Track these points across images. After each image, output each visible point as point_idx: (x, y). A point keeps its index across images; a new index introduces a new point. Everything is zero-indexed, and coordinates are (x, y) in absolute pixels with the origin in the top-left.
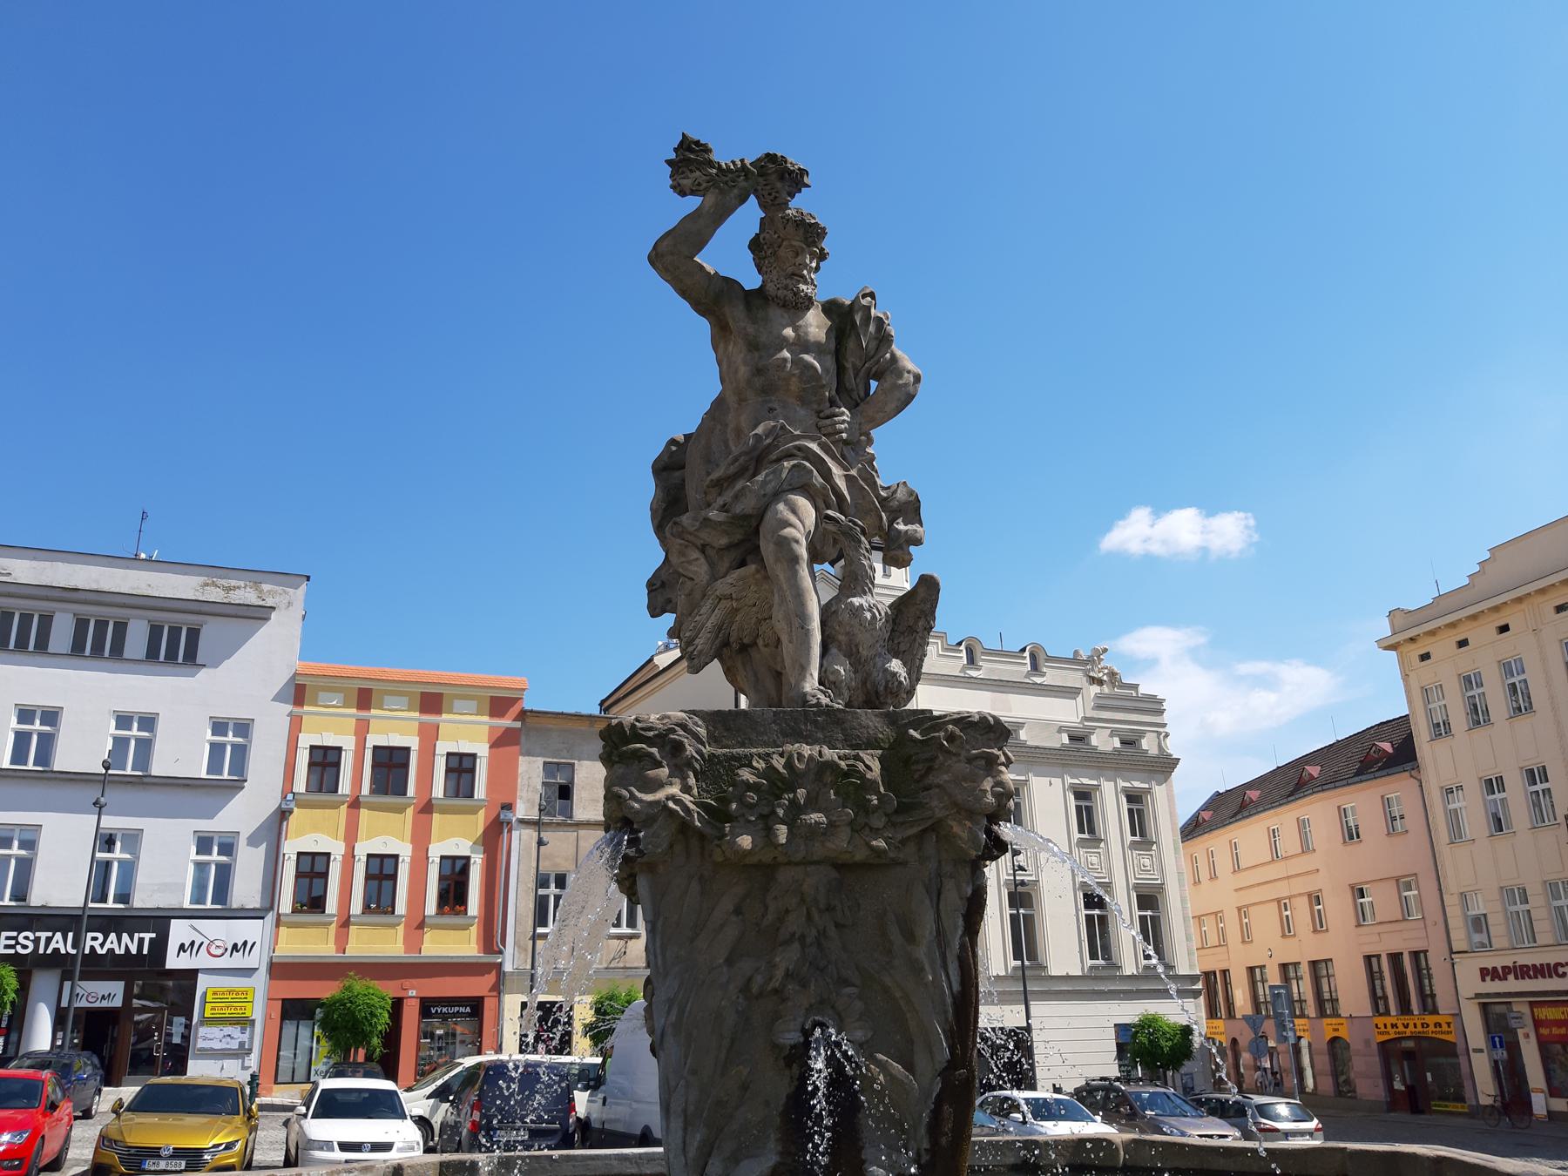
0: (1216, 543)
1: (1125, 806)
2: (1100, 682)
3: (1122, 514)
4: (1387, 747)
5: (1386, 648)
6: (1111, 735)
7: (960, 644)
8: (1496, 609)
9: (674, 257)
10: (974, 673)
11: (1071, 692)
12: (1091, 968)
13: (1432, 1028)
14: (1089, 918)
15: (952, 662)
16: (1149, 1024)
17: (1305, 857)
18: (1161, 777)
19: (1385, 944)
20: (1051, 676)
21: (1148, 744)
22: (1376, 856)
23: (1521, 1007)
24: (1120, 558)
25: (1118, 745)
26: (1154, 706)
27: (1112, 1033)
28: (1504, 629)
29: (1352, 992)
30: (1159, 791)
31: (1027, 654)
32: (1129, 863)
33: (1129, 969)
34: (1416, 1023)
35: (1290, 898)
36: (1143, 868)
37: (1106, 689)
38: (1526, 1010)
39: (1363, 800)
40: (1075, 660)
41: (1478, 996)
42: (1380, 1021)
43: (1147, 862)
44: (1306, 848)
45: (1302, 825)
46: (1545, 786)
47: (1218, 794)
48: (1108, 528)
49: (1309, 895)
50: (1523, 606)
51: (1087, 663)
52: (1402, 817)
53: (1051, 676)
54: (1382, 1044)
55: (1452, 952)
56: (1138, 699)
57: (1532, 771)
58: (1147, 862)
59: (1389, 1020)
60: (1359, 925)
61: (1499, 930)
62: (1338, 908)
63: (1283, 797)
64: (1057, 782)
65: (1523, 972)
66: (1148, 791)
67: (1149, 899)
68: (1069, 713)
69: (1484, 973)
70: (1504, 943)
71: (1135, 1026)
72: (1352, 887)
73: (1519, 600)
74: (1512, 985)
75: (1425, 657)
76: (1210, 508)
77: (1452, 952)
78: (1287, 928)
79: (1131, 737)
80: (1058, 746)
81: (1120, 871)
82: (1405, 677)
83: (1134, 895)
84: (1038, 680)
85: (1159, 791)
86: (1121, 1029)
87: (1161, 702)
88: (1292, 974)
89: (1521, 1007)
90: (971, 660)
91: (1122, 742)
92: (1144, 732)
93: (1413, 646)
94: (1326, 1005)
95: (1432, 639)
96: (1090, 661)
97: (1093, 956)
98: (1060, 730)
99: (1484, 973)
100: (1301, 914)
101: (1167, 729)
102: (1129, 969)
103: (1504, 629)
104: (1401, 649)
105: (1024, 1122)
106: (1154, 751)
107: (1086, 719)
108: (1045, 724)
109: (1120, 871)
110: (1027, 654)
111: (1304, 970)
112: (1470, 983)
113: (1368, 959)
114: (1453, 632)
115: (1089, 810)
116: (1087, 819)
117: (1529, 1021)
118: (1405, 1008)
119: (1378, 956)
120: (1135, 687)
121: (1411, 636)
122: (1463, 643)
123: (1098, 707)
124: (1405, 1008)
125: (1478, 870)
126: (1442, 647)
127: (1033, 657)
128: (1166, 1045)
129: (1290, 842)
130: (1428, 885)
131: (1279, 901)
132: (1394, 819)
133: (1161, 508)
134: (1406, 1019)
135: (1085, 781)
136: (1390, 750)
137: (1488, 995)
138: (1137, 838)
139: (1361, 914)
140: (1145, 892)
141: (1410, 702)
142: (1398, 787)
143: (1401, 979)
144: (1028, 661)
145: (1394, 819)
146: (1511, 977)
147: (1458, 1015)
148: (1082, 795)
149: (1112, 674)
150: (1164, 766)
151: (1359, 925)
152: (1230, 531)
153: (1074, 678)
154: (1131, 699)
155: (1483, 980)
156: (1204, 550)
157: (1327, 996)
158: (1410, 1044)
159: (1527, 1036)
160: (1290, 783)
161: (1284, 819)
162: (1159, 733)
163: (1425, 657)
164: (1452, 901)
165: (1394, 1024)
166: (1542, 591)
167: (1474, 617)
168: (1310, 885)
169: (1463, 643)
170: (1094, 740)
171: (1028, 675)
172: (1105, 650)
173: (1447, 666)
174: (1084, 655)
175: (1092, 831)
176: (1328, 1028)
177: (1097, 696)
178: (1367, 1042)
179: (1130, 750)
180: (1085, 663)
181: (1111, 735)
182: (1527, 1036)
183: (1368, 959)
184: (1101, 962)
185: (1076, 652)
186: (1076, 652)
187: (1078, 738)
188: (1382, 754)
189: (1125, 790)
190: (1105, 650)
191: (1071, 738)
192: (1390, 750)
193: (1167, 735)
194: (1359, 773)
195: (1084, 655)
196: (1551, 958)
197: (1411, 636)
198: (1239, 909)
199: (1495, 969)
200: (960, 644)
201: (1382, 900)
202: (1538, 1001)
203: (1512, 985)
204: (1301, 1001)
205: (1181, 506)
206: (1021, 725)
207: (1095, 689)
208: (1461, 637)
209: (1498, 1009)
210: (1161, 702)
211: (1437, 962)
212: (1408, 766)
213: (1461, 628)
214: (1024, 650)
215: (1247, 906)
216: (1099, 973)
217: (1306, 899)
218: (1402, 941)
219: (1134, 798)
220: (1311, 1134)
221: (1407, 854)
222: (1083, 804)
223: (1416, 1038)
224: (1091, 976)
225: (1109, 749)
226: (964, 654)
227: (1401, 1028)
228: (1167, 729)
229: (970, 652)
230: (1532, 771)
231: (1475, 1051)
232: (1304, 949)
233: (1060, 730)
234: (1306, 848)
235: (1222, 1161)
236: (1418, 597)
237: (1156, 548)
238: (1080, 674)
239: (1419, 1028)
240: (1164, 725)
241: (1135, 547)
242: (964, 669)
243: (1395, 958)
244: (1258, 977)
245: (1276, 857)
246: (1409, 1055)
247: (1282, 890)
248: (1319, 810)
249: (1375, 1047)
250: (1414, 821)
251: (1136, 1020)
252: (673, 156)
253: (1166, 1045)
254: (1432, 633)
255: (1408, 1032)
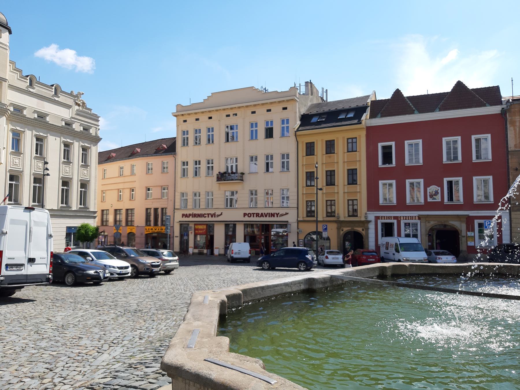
0: (80, 65)
2: (79, 105)
3: (48, 45)
4: (165, 146)
6: (80, 126)
7: (27, 76)
8: (210, 111)
11: (68, 107)
12: (61, 207)
14: (63, 190)
15: (23, 83)
17: (132, 177)
20: (62, 99)
21: (92, 131)
22: (157, 178)
23: (192, 225)
24: (42, 60)
25: (82, 129)
27: (65, 229)
28: (210, 118)
29: (139, 219)
30: (93, 148)
31: (54, 88)
32: (80, 172)
33: (74, 208)
35: (123, 189)
37: (81, 108)
38: (193, 226)
39: (156, 161)
40: (71, 94)
41: (180, 222)
42: (147, 228)
43: (86, 172)
44: (132, 174)
45: (132, 166)
49: (131, 189)
50: (218, 112)
52: (152, 169)
53: (62, 99)
54: (146, 235)
55: (175, 209)
58: (86, 172)
59: (150, 228)
61: (190, 205)
62: (140, 193)
64: (58, 139)
65: (195, 215)
67: (84, 185)
68: (66, 114)
69: (183, 215)
70: (191, 207)
71: (79, 227)
72: (146, 187)
73: (217, 110)
74: (191, 219)
75: (185, 121)
76: (80, 53)
78: (120, 198)
79: (87, 127)
80: (60, 126)
81: (76, 174)
82: (178, 126)
84: (57, 99)
85: (93, 148)
86: (69, 228)
89: (192, 225)
90: (31, 84)
91: (84, 129)
92: (92, 127)
93: (182, 117)
97: (62, 203)
98: (62, 120)
99: (183, 215)
100: (126, 194)
101: (99, 127)
102: (74, 208)
103: (210, 118)
104: (178, 117)
105: (93, 260)
106: (94, 134)
107: (72, 118)
108: (56, 116)
109: (76, 174)
111: (124, 212)
112: (178, 217)
113: (147, 209)
114: (195, 115)
115: (68, 151)
117: (193, 229)
118: (156, 224)
119: (150, 209)
120: (90, 110)
121: (182, 114)
122: (197, 119)
123: (77, 114)
124: (156, 224)
125: (187, 185)
126: (191, 119)
127: (56, 89)
129: (127, 171)
130: (171, 190)
131: (118, 189)
132: (149, 169)
133: (62, 47)
134: (156, 227)
135: (69, 140)
137: (183, 222)
138: (83, 164)
139: (147, 196)
140: (83, 182)
141: (177, 134)
142: (168, 159)
143: (155, 216)
145: (149, 169)
146: (191, 217)
147: (173, 227)
148: (67, 145)
149: (84, 103)
150: (96, 140)
152: (86, 63)
153: (69, 101)
154: (88, 113)
155: (244, 217)
156: (75, 67)
158: (156, 235)
159: (191, 233)
160: (129, 152)
161: (127, 164)
162: (96, 128)
163: (185, 121)
165: (152, 229)
166: (224, 109)
167: (203, 112)
168: (131, 186)
169: (197, 119)
170: (74, 126)
172: (83, 94)
173: (191, 126)
174: (75, 93)
175: (68, 159)
176: (128, 230)
177: (77, 110)
178: (142, 234)
179: (85, 131)
181: (80, 126)
182: (191, 233)
183: (147, 209)
186: (72, 92)
187: (68, 124)
188: (166, 148)
189: (82, 146)
190: (83, 94)
191: (66, 124)
193: (99, 129)
194: (155, 153)
195: (75, 93)
196: (203, 212)
197: (182, 114)
198: (102, 191)
199: (187, 214)
200: (27, 76)
201: (155, 193)
202: (196, 223)
203: (191, 219)
204: (120, 221)
205: (71, 49)
207: (77, 107)
208: (197, 118)
209: (185, 225)
210: (99, 117)
211: (169, 212)
212: (173, 153)
213: (197, 115)
214: (53, 85)
217: (117, 191)
218: (159, 205)
219: (85, 149)
220: (176, 260)
221: (167, 180)
222: (66, 149)
224: (61, 209)
226: (28, 81)
227: (154, 230)
228: (99, 127)
231: (176, 237)
232: (124, 205)
233: (62, 120)
234: (132, 174)
236: (186, 103)
237: (56, 60)
238: (72, 101)
239: (160, 230)
240: (98, 126)
241: (48, 58)
242: (27, 87)
243: (156, 210)
244: (164, 212)
245: (121, 175)
246: (154, 238)
247: (121, 186)
248: (139, 164)
249: (144, 235)
250: (171, 169)
254: (189, 114)
255: (156, 231)
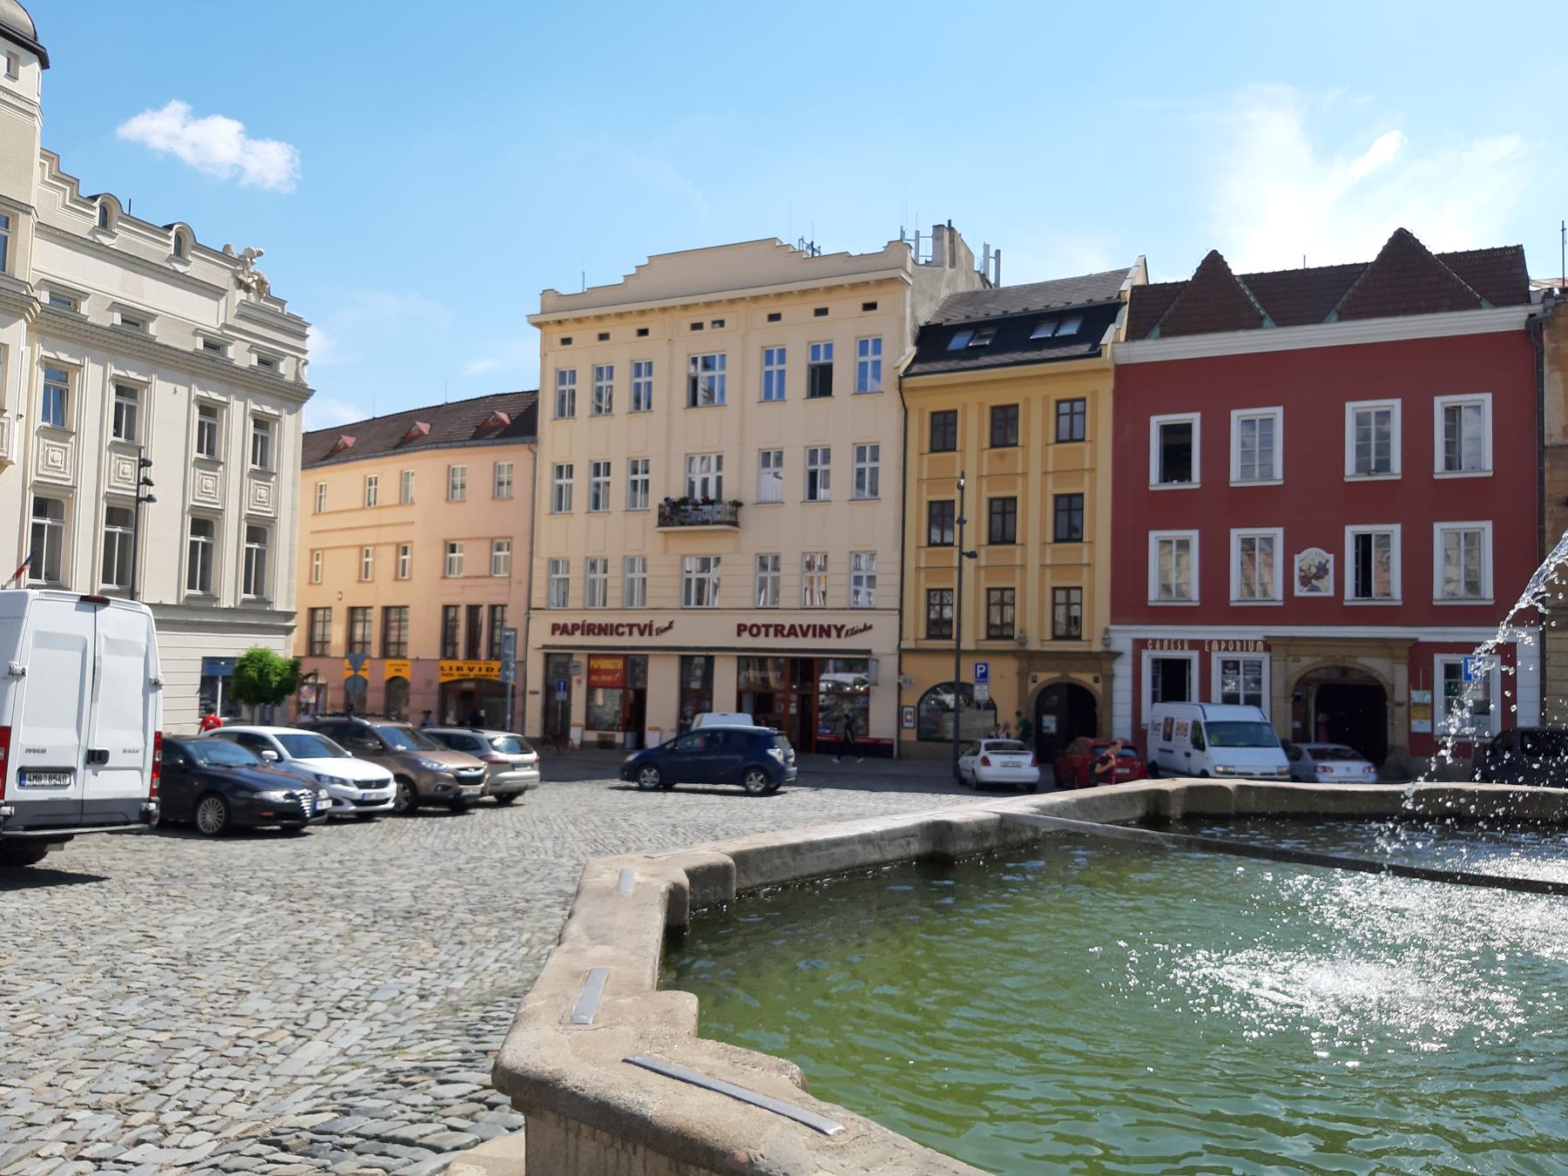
0: (253, 166)
1: (251, 430)
2: (247, 288)
3: (158, 105)
4: (504, 417)
5: (535, 324)
6: (250, 351)
7: (94, 198)
8: (642, 313)
10: (106, 241)
11: (216, 292)
12: (189, 598)
13: (496, 672)
14: (194, 545)
15: (79, 219)
16: (257, 660)
17: (402, 509)
18: (293, 406)
19: (463, 596)
20: (196, 268)
21: (286, 368)
22: (477, 516)
23: (580, 658)
24: (139, 148)
26: (297, 328)
27: (198, 666)
28: (643, 332)
29: (422, 638)
30: (288, 420)
31: (172, 234)
33: (227, 601)
34: (484, 667)
35: (375, 545)
36: (259, 499)
37: (253, 298)
38: (584, 660)
39: (476, 464)
40: (224, 255)
41: (545, 647)
42: (447, 664)
44: (405, 500)
45: (405, 477)
46: (607, 479)
48: (135, 111)
49: (398, 545)
50: (666, 316)
51: (237, 262)
52: (463, 486)
53: (196, 268)
54: (443, 686)
55: (530, 608)
56: (281, 317)
57: (636, 462)
58: (263, 493)
59: (455, 664)
60: (360, 581)
61: (576, 596)
62: (425, 560)
63: (388, 448)
64: (183, 390)
65: (589, 629)
66: (277, 418)
67: (258, 531)
68: (208, 315)
69: (555, 628)
71: (242, 660)
72: (445, 542)
73: (664, 310)
74: (578, 639)
76: (255, 130)
77: (530, 608)
78: (364, 573)
79: (269, 356)
80: (191, 350)
82: (544, 356)
83: (244, 526)
85: (288, 420)
86: (210, 662)
87: (305, 325)
88: (360, 617)
91: (260, 361)
92: (285, 355)
93: (557, 328)
94: (391, 648)
95: (578, 326)
96: (241, 261)
97: (191, 586)
98: (196, 333)
99: (555, 628)
100: (385, 562)
101: (307, 357)
102: (227, 601)
103: (643, 332)
105: (281, 759)
106: (290, 378)
108: (178, 322)
109: (234, 499)
110: (172, 234)
111: (376, 616)
112: (540, 634)
113: (446, 608)
115: (212, 428)
117: (584, 669)
118: (472, 653)
119: (456, 607)
120: (282, 303)
121: (559, 318)
123: (241, 316)
124: (472, 653)
125: (569, 537)
126: (584, 336)
128: (275, 679)
129: (388, 491)
130: (520, 549)
131: (361, 547)
133: (201, 111)
134: (472, 663)
135: (214, 396)
136: (508, 421)
139: (448, 567)
140: (255, 523)
141: (543, 380)
142: (512, 456)
143: (473, 629)
144: (172, 242)
145: (454, 487)
146: (578, 633)
147: (524, 662)
148: (208, 410)
149: (261, 283)
150: (297, 395)
151: (444, 577)
152: (271, 162)
153: (219, 276)
156: (238, 170)
157: (318, 638)
158: (471, 685)
159: (579, 682)
160: (396, 435)
161: (387, 470)
162: (299, 359)
163: (566, 341)
164: (540, 567)
165: (460, 668)
166: (685, 307)
167: (620, 315)
168: (402, 536)
169: (603, 337)
170: (231, 352)
171: (169, 260)
172: (260, 254)
173: (583, 357)
174: (236, 252)
175: (210, 451)
176: (389, 669)
177: (242, 304)
178: (429, 683)
180: (235, 261)
181: (250, 351)
182: (579, 682)
183: (446, 608)
184: (198, 592)
185: (227, 247)
186: (227, 247)
188: (508, 422)
190: (260, 254)
191: (206, 345)
192: (508, 421)
193: (306, 363)
194: (475, 437)
195: (236, 252)
197: (559, 318)
198: (312, 551)
199: (565, 626)
200: (94, 198)
201: (472, 558)
203: (578, 639)
204: (364, 643)
205: (227, 115)
206: (152, 317)
207: (241, 295)
209: (558, 659)
210: (305, 325)
211: (513, 618)
212: (527, 439)
214: (170, 227)
215: (323, 549)
216: (193, 603)
218: (483, 596)
221: (508, 519)
222: (207, 420)
223: (477, 680)
224: (188, 605)
225: (245, 365)
226: (97, 213)
227: (466, 671)
228: (307, 357)
229: (104, 213)
230: (636, 462)
232: (379, 595)
233: (196, 333)
234: (405, 500)
235: (1331, 804)
236: (570, 286)
237: (184, 151)
238: (228, 274)
239: (484, 672)
240: (304, 352)
241: (158, 142)
242: (93, 231)
243: (473, 610)
244: (498, 616)
245: (370, 503)
246: (466, 696)
247: (367, 537)
248: (425, 469)
249: (435, 687)
250: (520, 487)
251: (242, 654)
253: (275, 679)
254: (579, 320)
255: (472, 675)
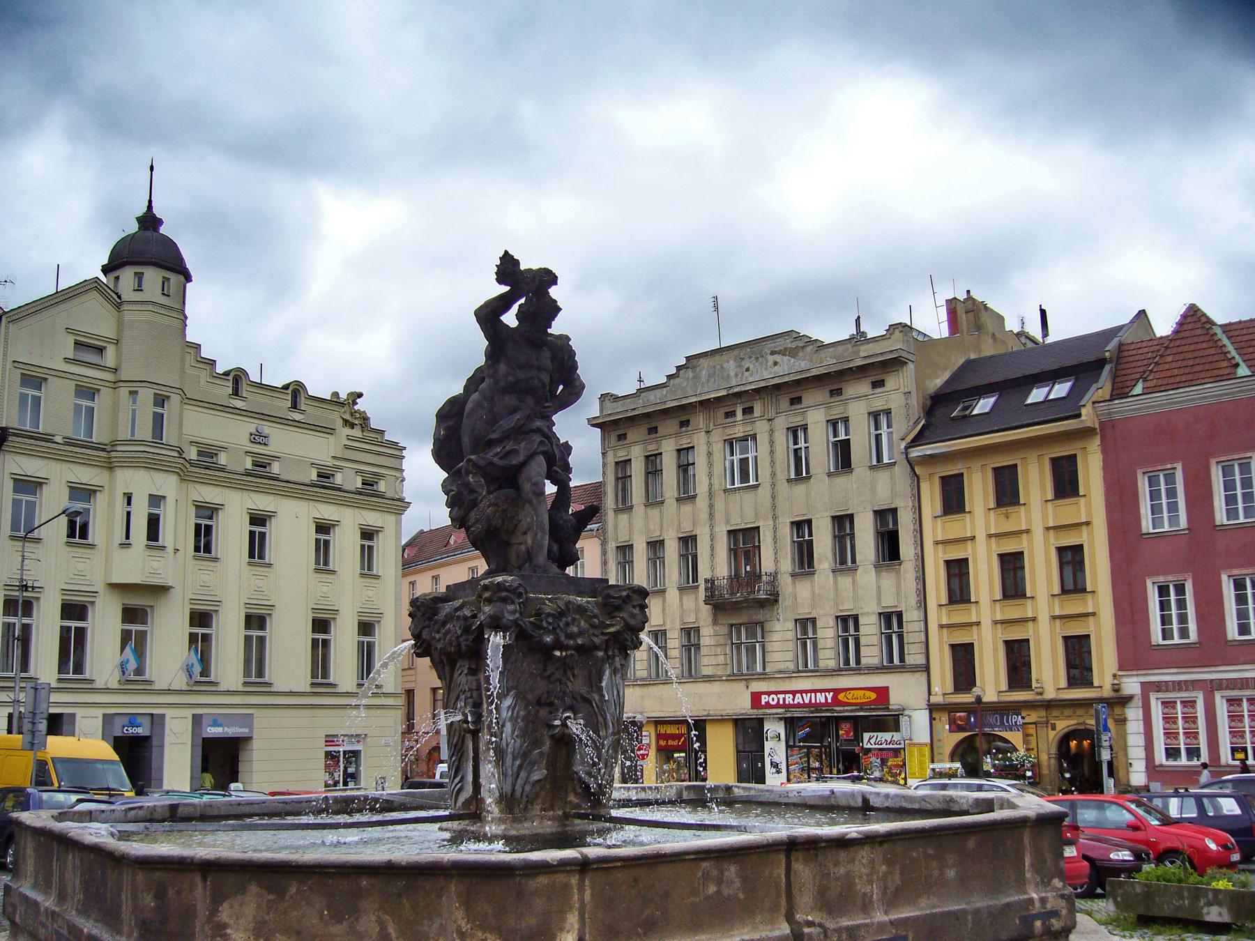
2: (352, 426)
9: (489, 315)
20: (311, 413)
47: (422, 532)
116: (323, 550)
148: (323, 528)
153: (335, 417)
252: (554, 292)
